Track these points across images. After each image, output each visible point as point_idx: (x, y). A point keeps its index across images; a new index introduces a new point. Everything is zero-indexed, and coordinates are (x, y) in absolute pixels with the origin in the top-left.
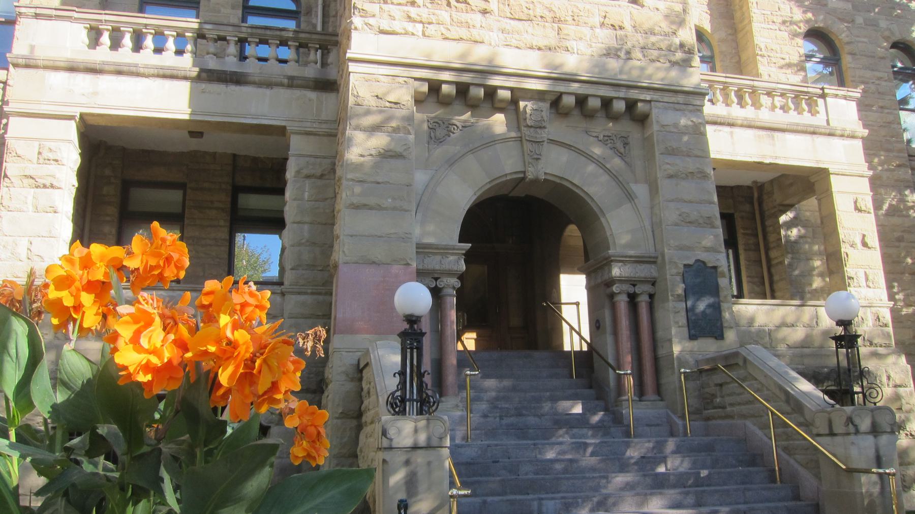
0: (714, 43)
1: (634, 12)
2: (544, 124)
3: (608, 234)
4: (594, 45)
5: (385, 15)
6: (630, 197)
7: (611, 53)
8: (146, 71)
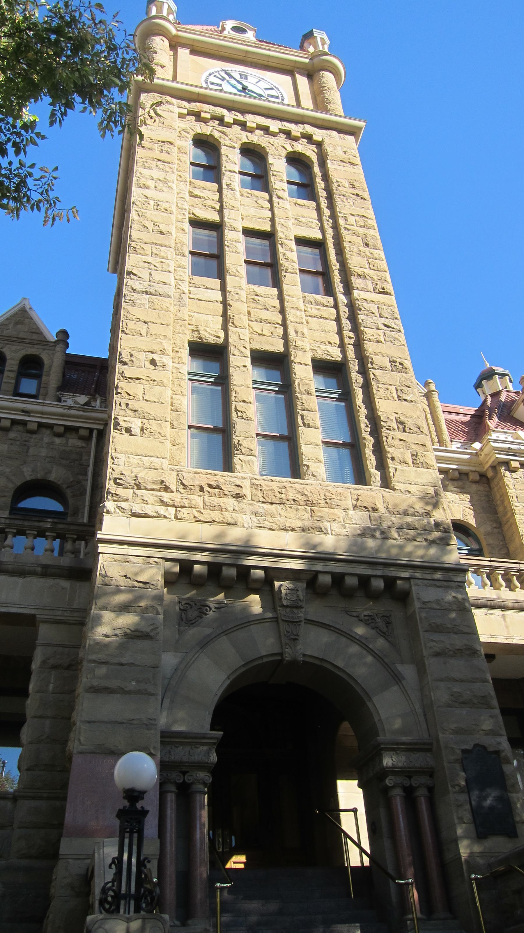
0: (481, 537)
1: (386, 495)
2: (300, 604)
3: (376, 719)
4: (347, 525)
5: (138, 500)
6: (397, 678)
7: (366, 533)
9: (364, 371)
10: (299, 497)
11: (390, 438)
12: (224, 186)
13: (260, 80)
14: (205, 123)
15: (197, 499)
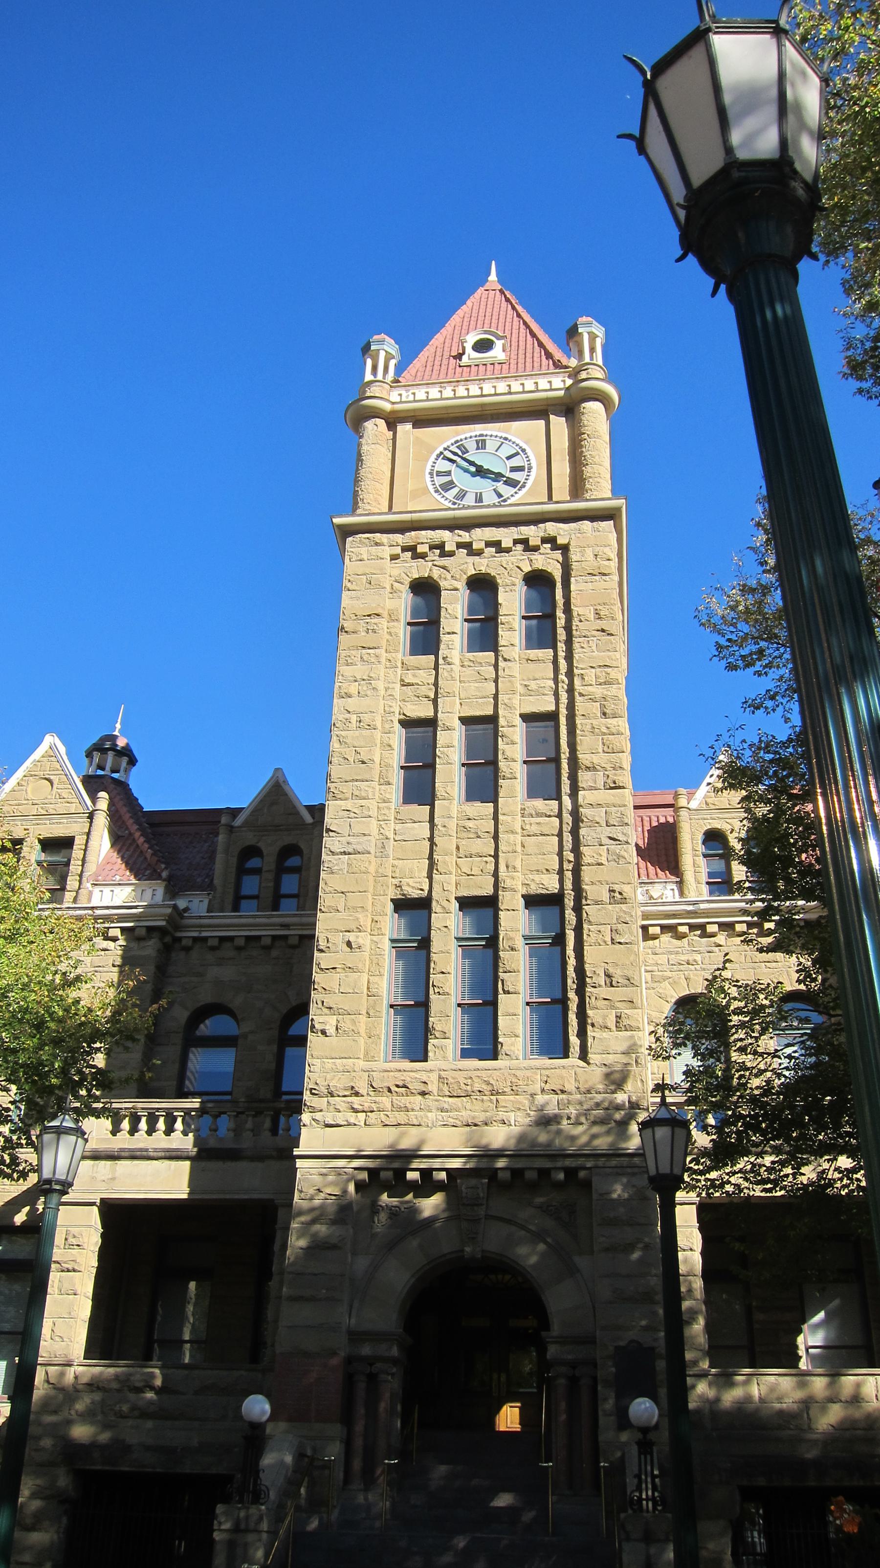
5: (331, 1108)
8: (155, 1154)
9: (578, 909)
10: (485, 1087)
11: (593, 999)
12: (441, 661)
13: (502, 443)
14: (423, 558)
15: (385, 1101)
